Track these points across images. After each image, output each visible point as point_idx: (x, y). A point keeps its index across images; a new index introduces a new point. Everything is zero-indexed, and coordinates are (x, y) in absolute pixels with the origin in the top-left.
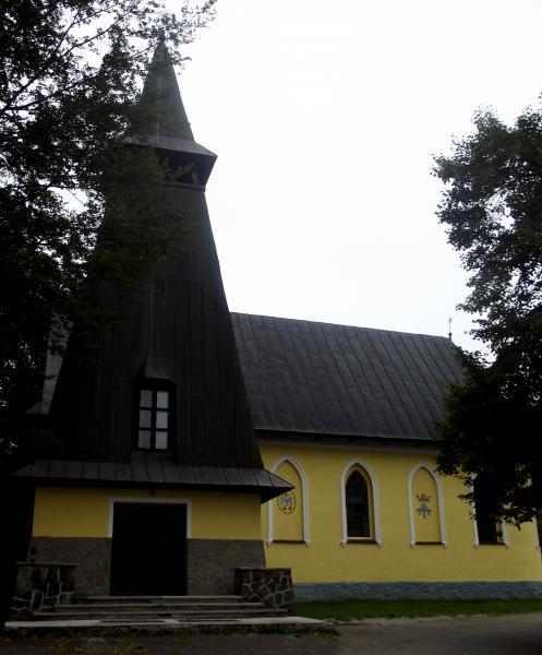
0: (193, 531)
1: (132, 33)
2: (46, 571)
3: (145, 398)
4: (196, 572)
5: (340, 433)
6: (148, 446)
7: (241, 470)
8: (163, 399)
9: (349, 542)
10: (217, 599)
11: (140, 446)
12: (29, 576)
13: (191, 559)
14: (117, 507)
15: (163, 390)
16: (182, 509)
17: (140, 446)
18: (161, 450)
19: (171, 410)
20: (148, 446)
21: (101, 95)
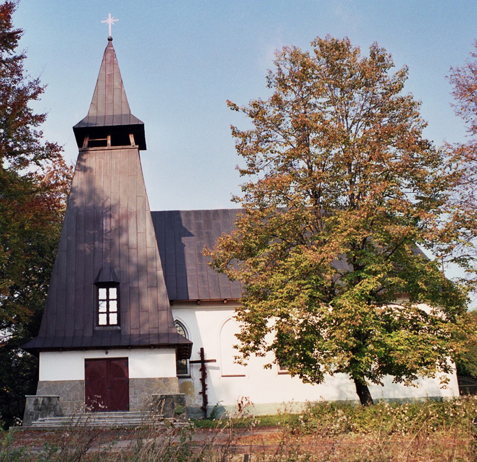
0: (132, 374)
1: (457, 166)
2: (42, 399)
3: (102, 293)
4: (133, 400)
5: (164, 281)
6: (105, 323)
7: (40, 328)
8: (113, 292)
9: (279, 374)
10: (136, 417)
11: (100, 323)
12: (33, 402)
13: (131, 391)
14: (88, 362)
15: (113, 287)
16: (127, 358)
17: (100, 323)
18: (113, 325)
19: (118, 300)
20: (105, 323)
21: (286, 164)
